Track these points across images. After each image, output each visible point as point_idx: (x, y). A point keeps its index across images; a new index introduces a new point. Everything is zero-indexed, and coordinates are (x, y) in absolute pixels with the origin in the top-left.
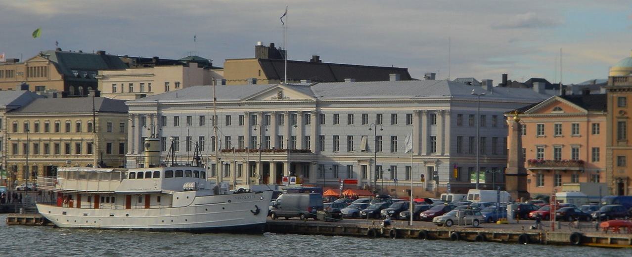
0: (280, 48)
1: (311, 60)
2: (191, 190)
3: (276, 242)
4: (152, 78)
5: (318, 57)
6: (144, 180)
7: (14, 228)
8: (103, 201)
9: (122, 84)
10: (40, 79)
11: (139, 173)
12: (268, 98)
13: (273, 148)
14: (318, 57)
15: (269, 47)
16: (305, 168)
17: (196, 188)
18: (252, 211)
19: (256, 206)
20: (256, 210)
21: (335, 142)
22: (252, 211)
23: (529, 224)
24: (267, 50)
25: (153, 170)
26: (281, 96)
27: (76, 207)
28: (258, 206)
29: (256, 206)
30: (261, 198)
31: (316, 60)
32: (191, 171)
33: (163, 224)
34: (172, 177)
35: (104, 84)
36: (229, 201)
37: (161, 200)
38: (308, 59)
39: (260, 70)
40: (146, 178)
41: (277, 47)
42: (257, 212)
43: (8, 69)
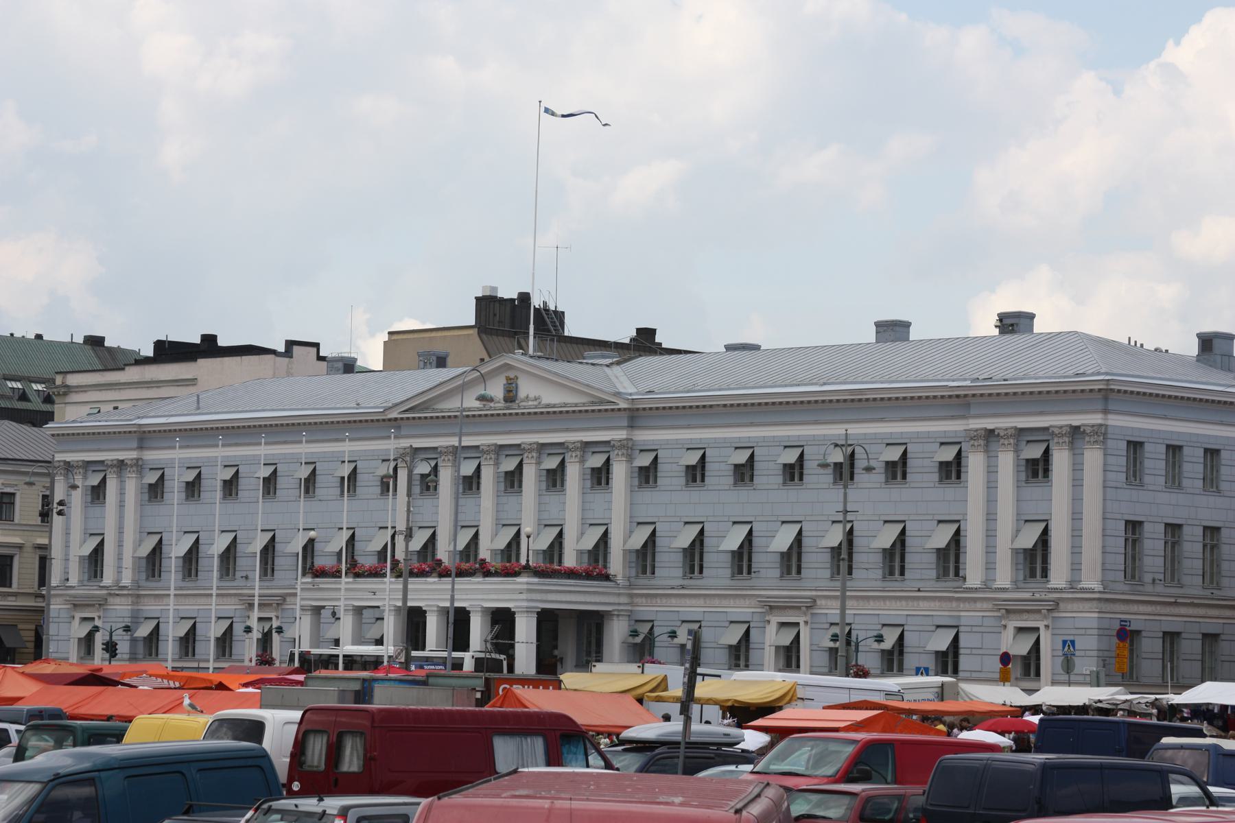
15: (513, 300)
24: (508, 309)
26: (511, 396)
35: (69, 409)
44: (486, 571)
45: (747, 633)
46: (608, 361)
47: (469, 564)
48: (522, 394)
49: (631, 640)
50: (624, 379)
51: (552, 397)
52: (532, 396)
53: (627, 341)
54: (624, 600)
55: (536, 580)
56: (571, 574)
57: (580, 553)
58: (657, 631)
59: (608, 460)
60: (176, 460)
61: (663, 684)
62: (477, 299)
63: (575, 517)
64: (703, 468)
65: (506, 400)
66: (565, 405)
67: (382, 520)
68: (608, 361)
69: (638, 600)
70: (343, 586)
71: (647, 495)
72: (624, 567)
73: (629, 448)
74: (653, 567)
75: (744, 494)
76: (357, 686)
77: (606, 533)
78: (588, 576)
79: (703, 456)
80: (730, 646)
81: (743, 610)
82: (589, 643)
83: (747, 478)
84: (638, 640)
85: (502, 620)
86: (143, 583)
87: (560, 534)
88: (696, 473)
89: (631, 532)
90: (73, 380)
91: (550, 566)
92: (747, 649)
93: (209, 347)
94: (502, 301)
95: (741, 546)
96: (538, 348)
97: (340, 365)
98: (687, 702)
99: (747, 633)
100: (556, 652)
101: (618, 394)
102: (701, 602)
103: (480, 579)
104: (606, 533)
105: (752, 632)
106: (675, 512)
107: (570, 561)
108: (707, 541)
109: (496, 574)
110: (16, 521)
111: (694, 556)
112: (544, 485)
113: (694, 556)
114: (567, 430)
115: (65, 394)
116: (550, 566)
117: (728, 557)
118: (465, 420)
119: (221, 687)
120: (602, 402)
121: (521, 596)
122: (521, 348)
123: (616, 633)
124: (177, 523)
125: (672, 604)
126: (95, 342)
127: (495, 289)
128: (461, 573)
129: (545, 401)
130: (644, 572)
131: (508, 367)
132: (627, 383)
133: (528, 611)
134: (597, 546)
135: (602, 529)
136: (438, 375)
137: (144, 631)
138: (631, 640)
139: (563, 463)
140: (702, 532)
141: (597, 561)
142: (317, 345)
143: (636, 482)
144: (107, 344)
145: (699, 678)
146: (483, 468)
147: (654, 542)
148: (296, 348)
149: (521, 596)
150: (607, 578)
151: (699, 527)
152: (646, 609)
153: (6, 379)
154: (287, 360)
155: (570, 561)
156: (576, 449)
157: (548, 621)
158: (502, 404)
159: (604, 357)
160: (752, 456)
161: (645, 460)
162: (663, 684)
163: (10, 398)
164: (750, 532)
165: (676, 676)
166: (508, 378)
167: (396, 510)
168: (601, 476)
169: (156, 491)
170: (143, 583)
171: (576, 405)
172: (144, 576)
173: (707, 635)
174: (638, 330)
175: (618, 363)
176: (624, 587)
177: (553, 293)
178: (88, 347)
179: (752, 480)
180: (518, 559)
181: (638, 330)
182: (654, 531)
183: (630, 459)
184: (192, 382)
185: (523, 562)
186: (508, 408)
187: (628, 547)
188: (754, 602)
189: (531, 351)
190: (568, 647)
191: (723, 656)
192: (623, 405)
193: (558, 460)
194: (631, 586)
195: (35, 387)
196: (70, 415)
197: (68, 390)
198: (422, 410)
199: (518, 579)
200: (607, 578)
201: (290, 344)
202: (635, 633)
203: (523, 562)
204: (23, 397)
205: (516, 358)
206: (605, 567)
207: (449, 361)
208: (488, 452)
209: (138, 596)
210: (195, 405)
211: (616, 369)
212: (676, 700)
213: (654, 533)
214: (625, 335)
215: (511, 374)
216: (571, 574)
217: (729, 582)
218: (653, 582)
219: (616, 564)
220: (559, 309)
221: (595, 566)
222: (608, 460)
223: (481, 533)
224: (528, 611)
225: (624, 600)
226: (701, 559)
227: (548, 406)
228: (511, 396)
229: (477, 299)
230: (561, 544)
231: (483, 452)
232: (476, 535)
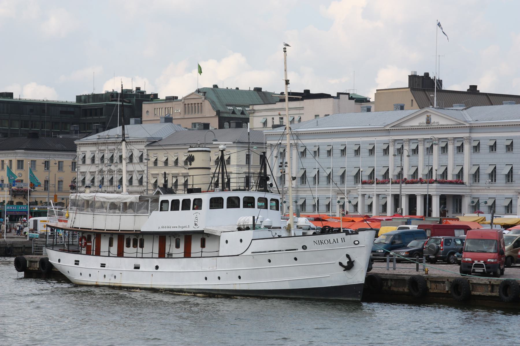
0: (435, 77)
1: (468, 90)
2: (248, 229)
3: (392, 319)
4: (301, 112)
5: (476, 87)
6: (180, 212)
7: (104, 289)
8: (128, 246)
9: (273, 118)
10: (197, 115)
11: (184, 201)
12: (415, 123)
13: (420, 179)
14: (476, 87)
15: (422, 77)
16: (457, 205)
17: (254, 224)
18: (341, 264)
19: (348, 256)
20: (348, 262)
21: (339, 108)
22: (341, 264)
23: (374, 216)
24: (421, 80)
25: (192, 197)
26: (428, 122)
27: (157, 256)
28: (351, 256)
29: (348, 256)
30: (357, 242)
31: (473, 89)
32: (266, 199)
33: (206, 282)
34: (223, 208)
35: (255, 118)
36: (304, 247)
37: (207, 244)
38: (469, 88)
39: (412, 100)
40: (182, 210)
41: (431, 76)
42: (350, 266)
43: (167, 107)
44: (421, 181)
45: (511, 202)
46: (462, 108)
47: (414, 180)
48: (432, 121)
49: (472, 204)
50: (467, 115)
51: (443, 122)
52: (436, 122)
53: (466, 91)
54: (468, 191)
55: (439, 185)
56: (451, 183)
57: (453, 175)
58: (480, 201)
59: (463, 143)
60: (310, 143)
61: (484, 219)
62: (409, 76)
63: (451, 162)
64: (495, 146)
65: (427, 123)
66: (448, 125)
67: (379, 164)
68: (462, 108)
69: (473, 191)
70: (375, 187)
71: (476, 155)
72: (469, 180)
73: (469, 139)
74: (479, 180)
75: (509, 155)
76: (406, 221)
77: (462, 168)
78: (456, 183)
79: (496, 142)
80: (506, 206)
81: (510, 194)
82: (457, 205)
83: (511, 149)
84: (474, 204)
85: (428, 200)
86: (300, 186)
87: (446, 169)
88: (493, 148)
89: (471, 168)
90: (256, 107)
91: (443, 180)
92: (511, 207)
93: (307, 95)
94: (419, 77)
95: (509, 173)
96: (438, 104)
97: (366, 109)
98: (491, 224)
99: (511, 202)
100: (446, 209)
101: (466, 121)
102: (495, 191)
103: (420, 185)
104: (462, 168)
105: (513, 201)
106: (486, 160)
107: (450, 178)
108: (497, 171)
109: (426, 183)
110: (399, 193)
111: (493, 175)
112: (440, 152)
113: (493, 175)
114: (448, 133)
115: (253, 113)
116: (443, 180)
117: (504, 176)
118: (413, 129)
119: (353, 221)
120: (460, 124)
121: (435, 191)
122: (431, 105)
123: (466, 203)
124: (311, 165)
125: (485, 192)
126: (258, 90)
127: (416, 72)
128: (413, 183)
129: (440, 124)
130: (476, 181)
131: (427, 112)
132: (469, 117)
133: (436, 195)
134: (459, 173)
135: (461, 167)
136: (401, 114)
137: (300, 202)
138: (472, 204)
139: (447, 144)
140: (495, 168)
141: (459, 178)
142: (348, 94)
143: (472, 151)
144: (262, 90)
145: (494, 218)
146: (419, 146)
147: (479, 171)
148: (341, 95)
149: (435, 191)
150: (463, 183)
151: (494, 166)
152: (476, 194)
153: (227, 106)
154: (337, 100)
155: (450, 178)
156: (451, 140)
157: (443, 199)
158: (425, 124)
159: (460, 106)
160: (512, 142)
161: (476, 144)
162: (484, 219)
163: (229, 113)
164: (512, 168)
165: (488, 217)
166: (427, 116)
167: (391, 161)
168: (460, 149)
169: (303, 154)
170: (300, 186)
171: (451, 125)
172: (300, 184)
173: (497, 203)
174: (470, 86)
175: (465, 109)
176: (469, 187)
177: (438, 73)
178: (256, 92)
179: (512, 150)
180: (432, 178)
181: (470, 86)
182: (479, 168)
183: (470, 143)
184: (302, 108)
185: (434, 178)
186: (428, 126)
187: (470, 173)
188: (513, 191)
189: (435, 106)
190: (450, 207)
191: (503, 210)
192: (468, 125)
193: (445, 144)
194: (471, 186)
195: (238, 108)
196: (255, 123)
197: (254, 111)
198: (397, 127)
199: (433, 185)
200: (463, 183)
201: (339, 94)
202: (473, 202)
203: (434, 178)
204: (234, 112)
205: (430, 109)
206: (462, 180)
207: (405, 107)
208: (421, 141)
209: (298, 191)
210: (316, 124)
211: (465, 111)
212: (489, 223)
213: (479, 168)
214: (465, 88)
215: (429, 114)
216: (451, 183)
217: (505, 185)
218: (479, 185)
219: (466, 179)
220: (440, 79)
221: (459, 180)
222: (463, 143)
223: (419, 168)
224: (436, 195)
225: (468, 191)
226: (495, 177)
227: (442, 125)
228: (428, 122)
229: (409, 76)
230: (447, 172)
231: (419, 141)
232: (417, 169)
